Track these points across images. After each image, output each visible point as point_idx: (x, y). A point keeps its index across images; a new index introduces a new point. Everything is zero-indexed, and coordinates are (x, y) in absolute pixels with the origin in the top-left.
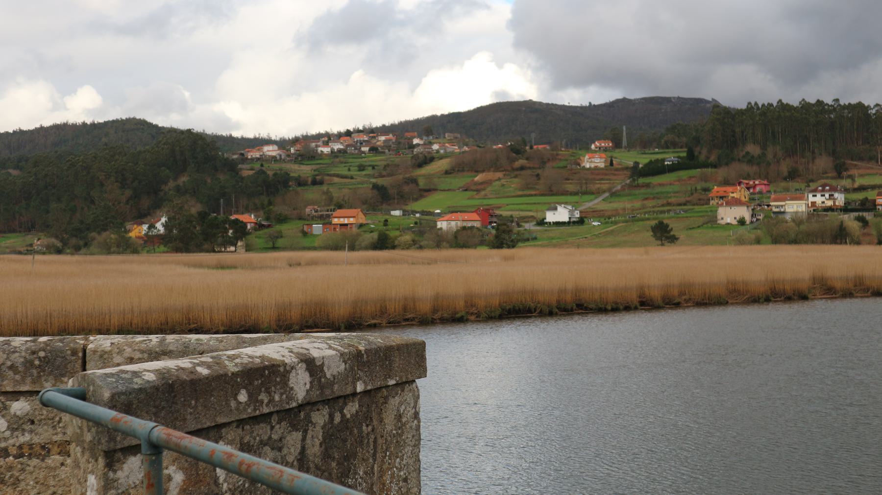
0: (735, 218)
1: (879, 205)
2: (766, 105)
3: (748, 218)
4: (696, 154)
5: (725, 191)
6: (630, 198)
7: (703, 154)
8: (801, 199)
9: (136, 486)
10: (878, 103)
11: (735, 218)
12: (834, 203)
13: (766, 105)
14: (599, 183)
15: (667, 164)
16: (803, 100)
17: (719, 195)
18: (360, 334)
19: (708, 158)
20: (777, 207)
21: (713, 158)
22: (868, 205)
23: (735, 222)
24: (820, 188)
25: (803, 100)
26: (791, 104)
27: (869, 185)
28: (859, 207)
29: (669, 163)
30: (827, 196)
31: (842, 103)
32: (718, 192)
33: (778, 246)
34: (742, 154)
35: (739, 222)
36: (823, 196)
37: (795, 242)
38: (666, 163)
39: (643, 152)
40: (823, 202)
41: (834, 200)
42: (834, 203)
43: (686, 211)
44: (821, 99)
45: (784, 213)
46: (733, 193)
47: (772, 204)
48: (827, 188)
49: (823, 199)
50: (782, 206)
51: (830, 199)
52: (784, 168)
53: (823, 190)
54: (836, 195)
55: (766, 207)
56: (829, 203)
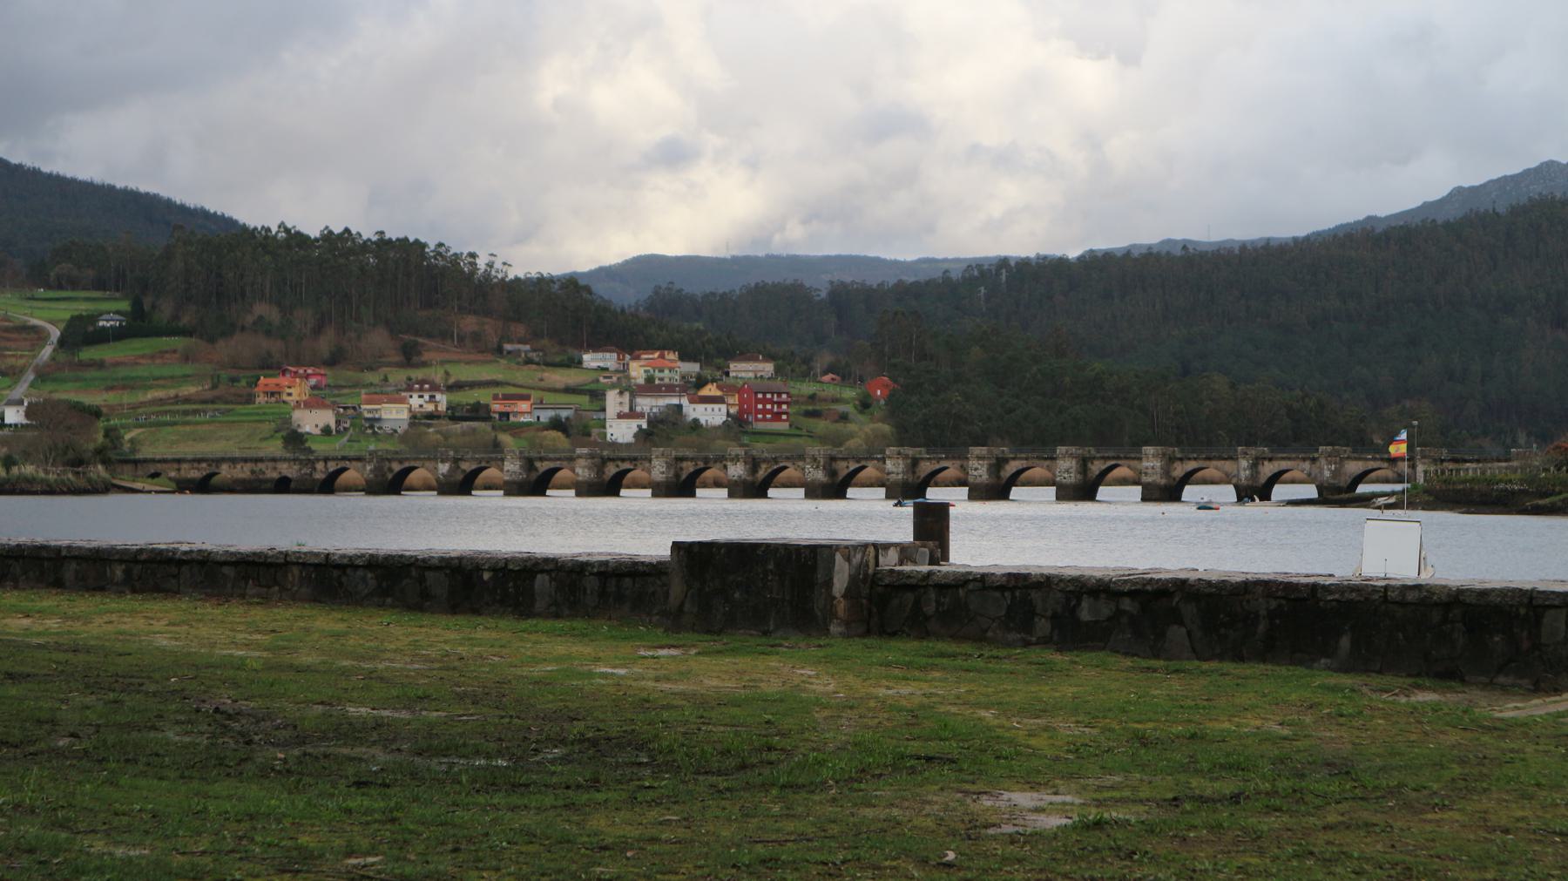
0: (317, 426)
1: (495, 412)
2: (259, 229)
3: (333, 426)
4: (146, 308)
5: (277, 385)
6: (78, 384)
7: (165, 311)
8: (402, 401)
9: (170, 873)
10: (442, 241)
11: (317, 426)
12: (436, 406)
13: (259, 229)
14: (13, 356)
15: (103, 326)
16: (327, 228)
17: (267, 389)
18: (1430, 697)
19: (176, 317)
20: (370, 411)
21: (186, 320)
22: (482, 413)
23: (317, 431)
24: (417, 386)
25: (327, 228)
26: (1032, 255)
27: (467, 382)
28: (468, 415)
29: (105, 323)
30: (427, 397)
31: (387, 236)
32: (266, 385)
33: (1148, 503)
34: (250, 319)
35: (322, 430)
36: (421, 397)
37: (868, 486)
38: (101, 324)
39: (29, 295)
40: (421, 406)
41: (436, 404)
42: (436, 406)
43: (223, 413)
44: (266, 226)
45: (379, 420)
46: (290, 387)
47: (363, 407)
48: (427, 386)
49: (421, 401)
50: (377, 410)
51: (430, 401)
52: (325, 344)
53: (421, 389)
54: (438, 397)
55: (341, 410)
56: (430, 408)
